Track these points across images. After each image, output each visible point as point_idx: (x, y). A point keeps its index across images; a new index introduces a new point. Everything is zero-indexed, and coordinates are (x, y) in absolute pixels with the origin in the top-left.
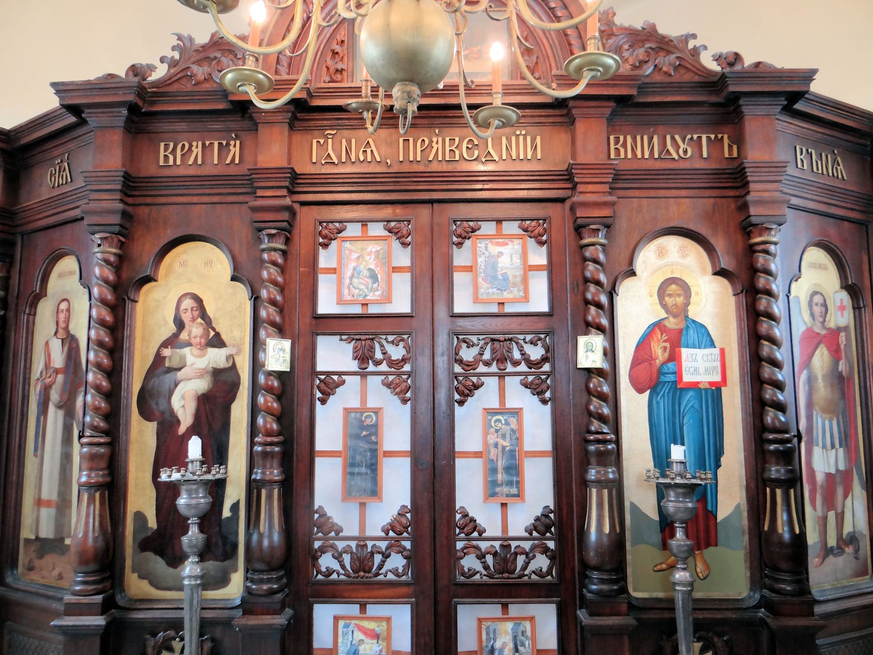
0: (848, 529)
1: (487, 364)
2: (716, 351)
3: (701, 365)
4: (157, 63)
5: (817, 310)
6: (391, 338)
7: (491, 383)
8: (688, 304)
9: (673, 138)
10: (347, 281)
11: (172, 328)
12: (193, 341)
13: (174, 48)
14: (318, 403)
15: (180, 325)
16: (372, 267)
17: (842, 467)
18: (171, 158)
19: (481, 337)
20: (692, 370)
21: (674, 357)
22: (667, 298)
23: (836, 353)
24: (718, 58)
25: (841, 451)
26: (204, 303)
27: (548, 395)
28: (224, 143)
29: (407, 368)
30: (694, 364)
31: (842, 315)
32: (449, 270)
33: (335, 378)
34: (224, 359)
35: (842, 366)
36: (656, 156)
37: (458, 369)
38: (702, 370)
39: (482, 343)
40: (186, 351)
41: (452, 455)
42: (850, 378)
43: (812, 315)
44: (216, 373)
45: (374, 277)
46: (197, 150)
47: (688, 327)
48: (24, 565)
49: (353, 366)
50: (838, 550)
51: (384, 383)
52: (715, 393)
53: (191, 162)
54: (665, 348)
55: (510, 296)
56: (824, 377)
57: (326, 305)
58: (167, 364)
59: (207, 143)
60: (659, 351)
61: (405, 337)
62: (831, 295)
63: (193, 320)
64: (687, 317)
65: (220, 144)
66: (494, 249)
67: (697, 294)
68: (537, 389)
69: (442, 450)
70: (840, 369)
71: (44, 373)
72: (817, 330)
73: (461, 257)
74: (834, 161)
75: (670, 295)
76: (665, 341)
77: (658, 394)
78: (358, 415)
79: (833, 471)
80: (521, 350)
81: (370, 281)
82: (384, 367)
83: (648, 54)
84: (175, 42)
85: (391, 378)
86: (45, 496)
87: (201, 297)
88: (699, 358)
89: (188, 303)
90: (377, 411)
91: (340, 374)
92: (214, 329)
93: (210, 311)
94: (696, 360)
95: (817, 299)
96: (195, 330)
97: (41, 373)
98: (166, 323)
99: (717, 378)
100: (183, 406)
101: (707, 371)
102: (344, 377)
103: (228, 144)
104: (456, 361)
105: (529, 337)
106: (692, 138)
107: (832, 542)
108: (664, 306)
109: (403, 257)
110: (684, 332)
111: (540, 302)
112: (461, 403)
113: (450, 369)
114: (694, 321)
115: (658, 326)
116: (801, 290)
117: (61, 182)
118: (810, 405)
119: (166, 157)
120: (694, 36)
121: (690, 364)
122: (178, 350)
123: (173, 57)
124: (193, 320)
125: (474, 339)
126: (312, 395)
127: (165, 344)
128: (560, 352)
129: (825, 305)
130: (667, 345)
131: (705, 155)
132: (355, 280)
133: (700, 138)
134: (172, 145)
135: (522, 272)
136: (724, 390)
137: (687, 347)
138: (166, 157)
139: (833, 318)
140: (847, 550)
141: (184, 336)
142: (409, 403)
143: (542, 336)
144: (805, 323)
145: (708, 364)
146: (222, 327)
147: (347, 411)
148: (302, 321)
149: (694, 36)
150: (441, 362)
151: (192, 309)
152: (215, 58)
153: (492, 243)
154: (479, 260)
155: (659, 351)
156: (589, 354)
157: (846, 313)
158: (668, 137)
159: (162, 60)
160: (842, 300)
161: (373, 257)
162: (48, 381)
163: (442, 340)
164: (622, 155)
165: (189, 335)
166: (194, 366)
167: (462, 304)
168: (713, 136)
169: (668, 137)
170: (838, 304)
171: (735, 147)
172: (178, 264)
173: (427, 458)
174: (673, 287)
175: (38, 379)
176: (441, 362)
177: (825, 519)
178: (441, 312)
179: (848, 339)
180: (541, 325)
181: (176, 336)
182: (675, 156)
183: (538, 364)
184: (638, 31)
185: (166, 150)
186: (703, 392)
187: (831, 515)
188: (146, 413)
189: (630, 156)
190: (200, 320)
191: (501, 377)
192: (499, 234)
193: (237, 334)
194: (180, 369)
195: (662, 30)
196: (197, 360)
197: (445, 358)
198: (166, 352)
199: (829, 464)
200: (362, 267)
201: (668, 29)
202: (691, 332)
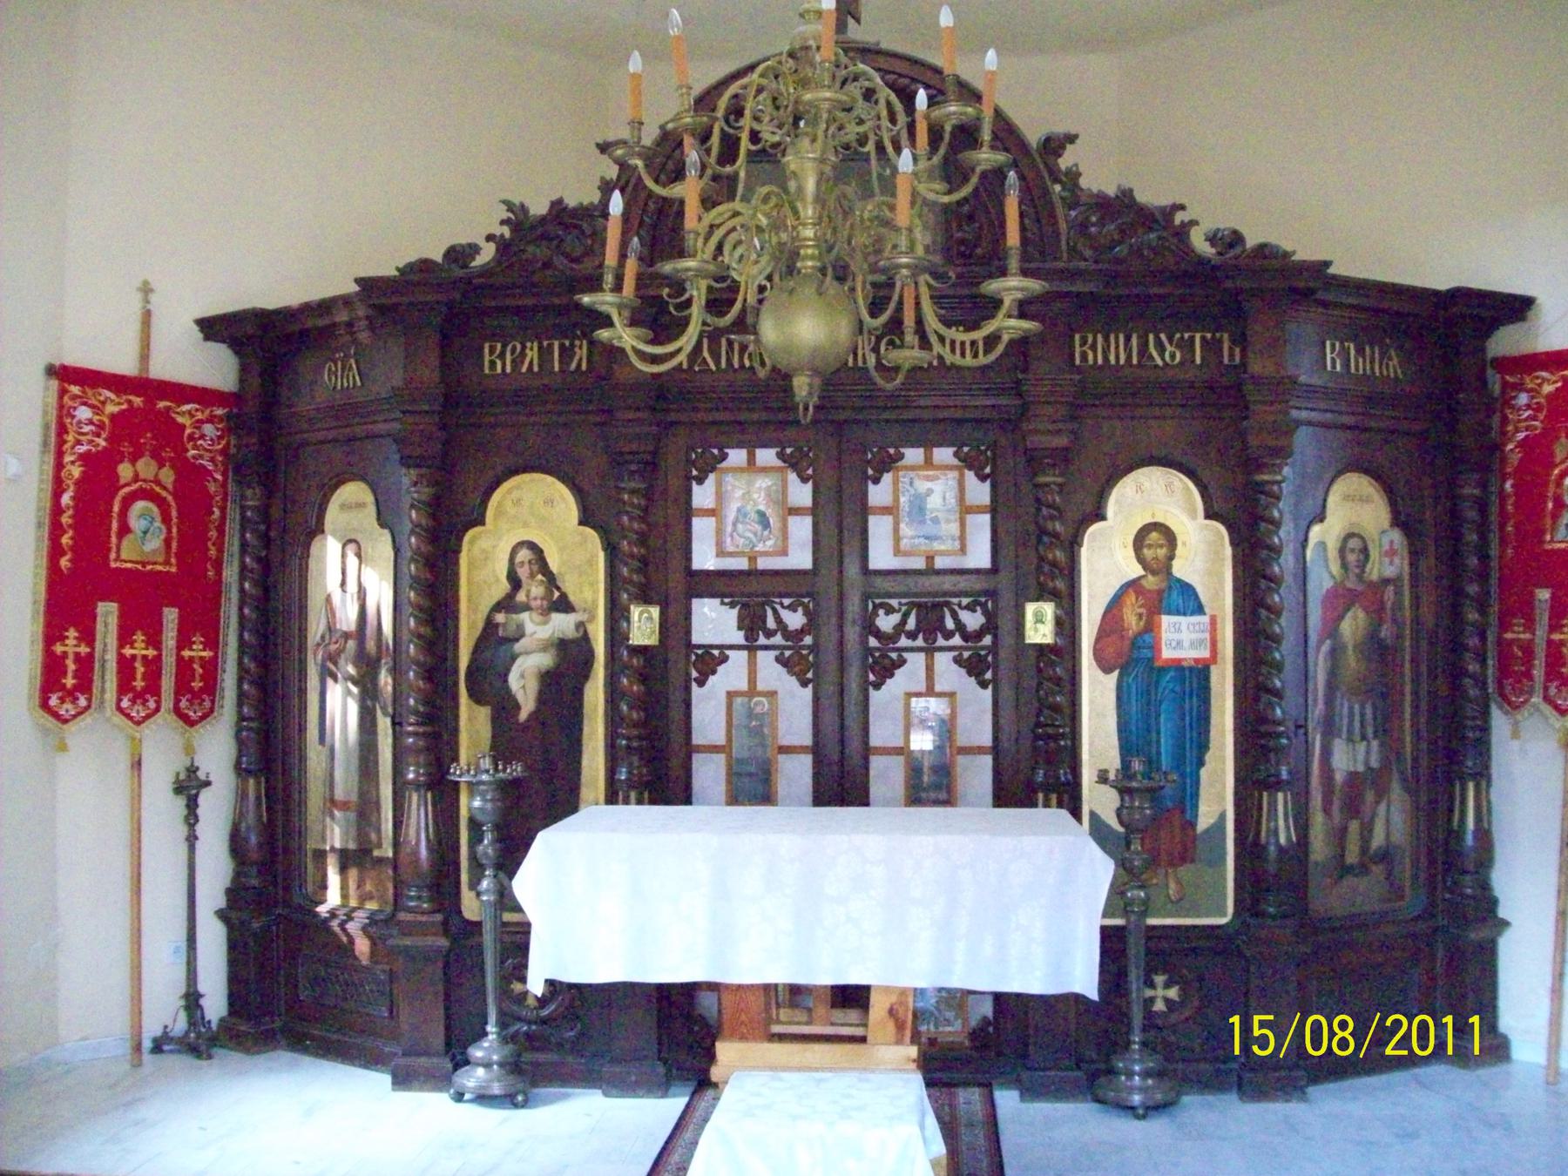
0: (1378, 840)
1: (912, 635)
2: (1205, 619)
3: (1186, 636)
4: (482, 243)
5: (1352, 558)
6: (787, 602)
7: (916, 661)
8: (1171, 557)
9: (1158, 339)
10: (729, 529)
11: (504, 587)
12: (534, 604)
13: (503, 222)
14: (694, 685)
15: (515, 582)
16: (762, 508)
17: (1375, 764)
18: (499, 364)
19: (904, 601)
20: (1174, 644)
21: (1151, 627)
22: (1145, 551)
23: (1377, 612)
24: (1212, 239)
25: (1375, 744)
26: (546, 554)
27: (988, 675)
28: (567, 343)
29: (808, 640)
30: (1176, 636)
31: (1391, 563)
32: (864, 510)
33: (716, 652)
34: (572, 627)
35: (1386, 632)
36: (1135, 361)
37: (873, 642)
38: (1186, 644)
39: (904, 608)
40: (525, 616)
41: (867, 751)
42: (1396, 650)
43: (1344, 565)
44: (562, 645)
45: (763, 519)
46: (532, 354)
47: (1170, 588)
48: (314, 883)
49: (738, 637)
50: (1363, 869)
51: (778, 659)
52: (1197, 677)
53: (524, 370)
54: (1140, 616)
55: (943, 547)
56: (1355, 647)
57: (705, 558)
58: (501, 633)
59: (545, 343)
60: (1132, 619)
61: (806, 600)
62: (1376, 537)
63: (532, 576)
64: (1169, 573)
65: (562, 346)
66: (922, 486)
67: (1184, 544)
68: (974, 667)
69: (854, 745)
70: (1383, 635)
71: (327, 637)
72: (1349, 585)
73: (878, 494)
74: (1383, 355)
75: (1150, 546)
76: (1140, 607)
77: (1130, 675)
78: (746, 699)
79: (1361, 768)
80: (955, 616)
81: (758, 528)
82: (778, 639)
83: (1122, 231)
84: (506, 215)
85: (787, 653)
86: (339, 794)
87: (541, 546)
88: (1184, 627)
89: (524, 555)
90: (772, 694)
91: (721, 647)
92: (558, 588)
93: (554, 564)
94: (1179, 630)
95: (1354, 543)
96: (534, 589)
97: (323, 637)
98: (498, 580)
99: (1205, 653)
100: (524, 687)
101: (1193, 645)
102: (727, 652)
103: (572, 345)
104: (871, 633)
105: (965, 601)
106: (1182, 338)
107: (1352, 857)
108: (1140, 559)
109: (802, 494)
110: (1166, 595)
111: (979, 555)
112: (877, 686)
113: (864, 642)
114: (1179, 581)
115: (1133, 585)
116: (1328, 534)
117: (346, 384)
118: (1331, 687)
119: (493, 364)
120: (1182, 207)
121: (1171, 636)
122: (514, 616)
123: (502, 236)
124: (532, 576)
125: (894, 602)
126: (688, 674)
127: (499, 607)
128: (1005, 624)
129: (1365, 551)
130: (1142, 610)
131: (1198, 361)
132: (740, 527)
133: (1192, 339)
134: (499, 346)
135: (958, 516)
136: (1213, 669)
137: (1169, 613)
138: (493, 364)
139: (1377, 565)
140: (1374, 868)
141: (521, 597)
142: (810, 686)
143: (983, 600)
144: (1333, 577)
145: (1194, 636)
146: (571, 586)
147: (731, 695)
148: (676, 581)
149: (1182, 207)
150: (852, 633)
151: (530, 562)
152: (558, 236)
153: (919, 476)
154: (902, 499)
155: (1132, 619)
156: (1039, 625)
157: (1397, 561)
158: (1151, 337)
159: (490, 238)
160: (1392, 542)
161: (763, 494)
162: (333, 647)
163: (853, 607)
164: (1091, 361)
165: (527, 596)
166: (536, 636)
167: (881, 557)
168: (1209, 336)
169: (1151, 337)
170: (1386, 547)
171: (1237, 350)
172: (510, 503)
173: (833, 751)
174: (1154, 535)
175: (318, 645)
176: (852, 633)
177: (1344, 830)
178: (852, 570)
179: (1398, 593)
180: (977, 584)
181: (510, 596)
182: (1159, 362)
183: (979, 635)
184: (1110, 198)
185: (492, 352)
186: (1187, 673)
187: (1354, 826)
188: (477, 697)
189: (1100, 361)
190: (540, 577)
191: (930, 651)
192: (928, 462)
193: (588, 594)
194: (517, 640)
195: (1142, 197)
196: (539, 629)
197: (857, 629)
198: (500, 618)
199: (1355, 761)
200: (749, 508)
201: (1150, 195)
202: (1175, 594)
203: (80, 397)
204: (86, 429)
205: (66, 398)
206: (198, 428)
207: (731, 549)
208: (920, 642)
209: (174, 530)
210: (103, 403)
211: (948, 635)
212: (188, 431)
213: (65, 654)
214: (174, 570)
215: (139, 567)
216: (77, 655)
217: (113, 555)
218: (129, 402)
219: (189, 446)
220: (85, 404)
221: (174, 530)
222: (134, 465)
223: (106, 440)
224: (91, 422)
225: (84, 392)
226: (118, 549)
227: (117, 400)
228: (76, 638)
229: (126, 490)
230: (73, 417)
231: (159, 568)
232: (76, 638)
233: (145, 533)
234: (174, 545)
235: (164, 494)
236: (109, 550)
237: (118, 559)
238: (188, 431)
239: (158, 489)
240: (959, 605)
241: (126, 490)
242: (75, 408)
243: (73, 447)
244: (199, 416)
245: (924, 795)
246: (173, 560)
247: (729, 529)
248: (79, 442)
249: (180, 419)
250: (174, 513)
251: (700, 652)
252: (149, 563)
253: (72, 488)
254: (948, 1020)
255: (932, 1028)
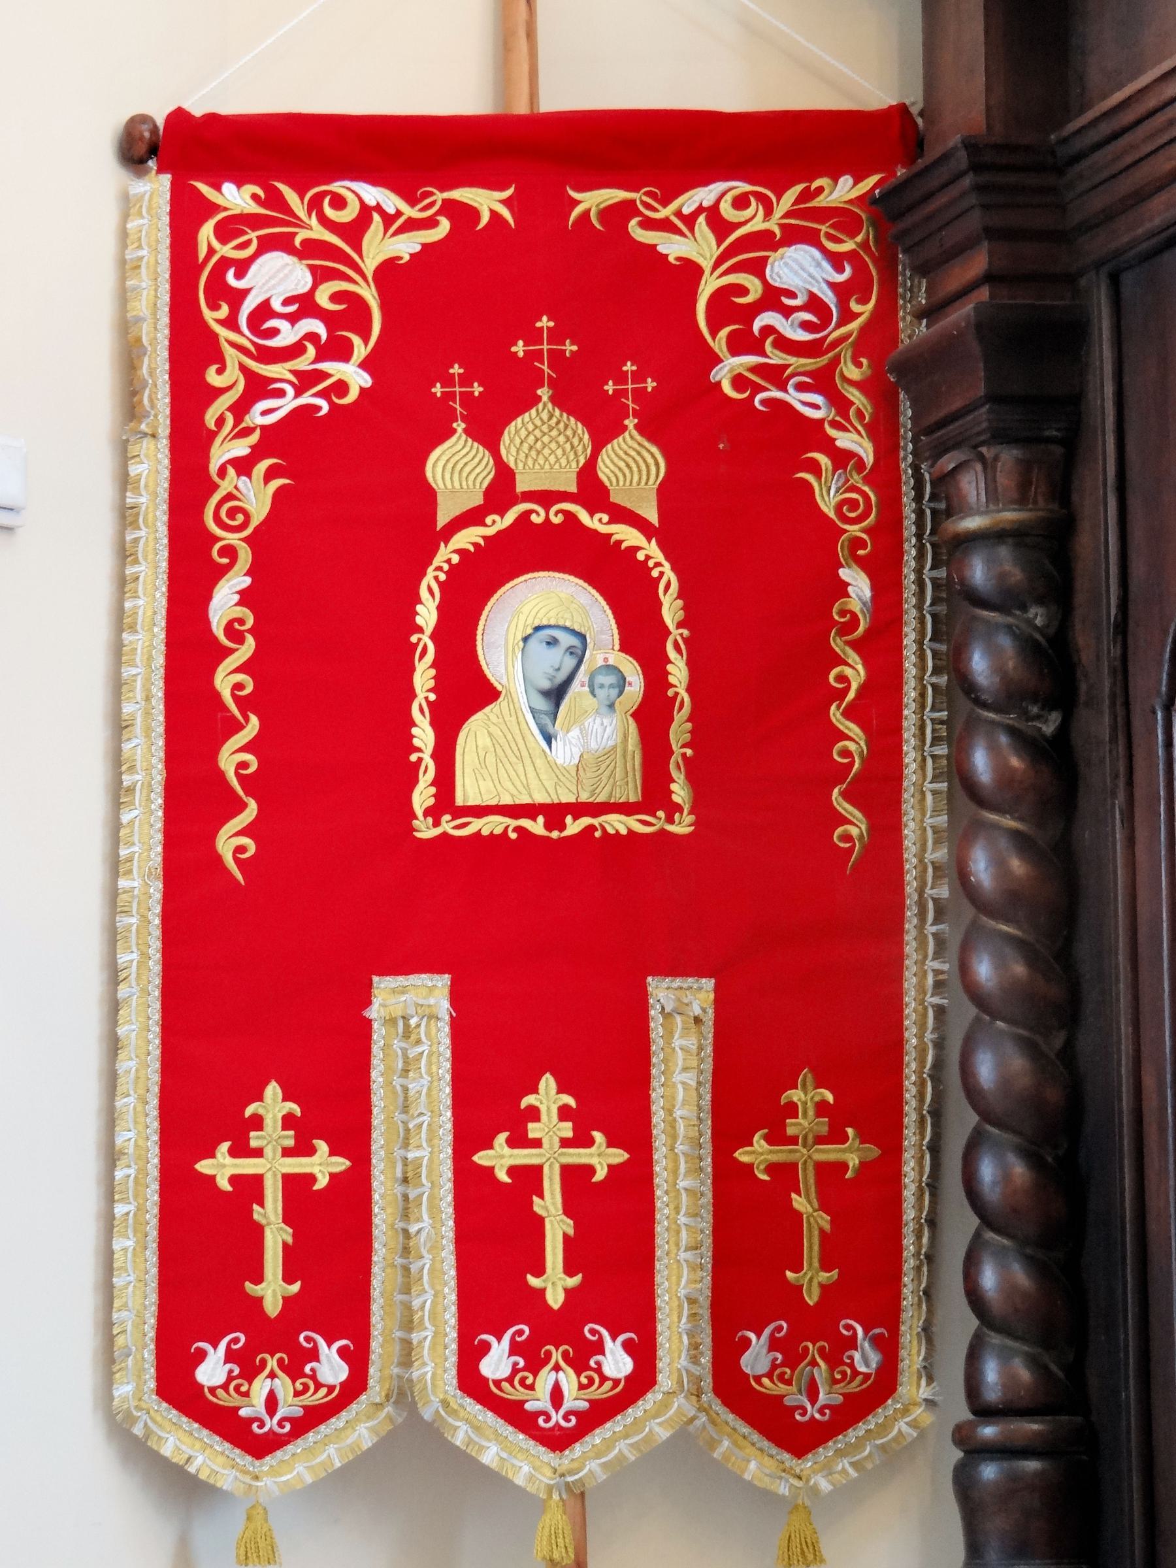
203: (253, 221)
204: (288, 335)
205: (207, 232)
206: (757, 268)
209: (678, 672)
210: (354, 232)
212: (709, 286)
213: (250, 1188)
214: (682, 826)
215: (537, 827)
216: (296, 1185)
217: (422, 796)
218: (462, 214)
219: (719, 343)
220: (283, 244)
221: (678, 672)
222: (491, 441)
223: (364, 365)
224: (305, 305)
225: (274, 200)
226: (445, 781)
227: (410, 212)
228: (564, 1113)
229: (467, 538)
230: (237, 298)
231: (617, 824)
232: (288, 1121)
233: (557, 694)
234: (679, 732)
235: (628, 535)
236: (411, 774)
237: (444, 802)
238: (709, 286)
239: (596, 522)
241: (467, 538)
242: (242, 268)
243: (240, 409)
244: (755, 221)
246: (680, 792)
248: (258, 388)
249: (673, 247)
250: (671, 610)
252: (579, 809)
253: (245, 556)
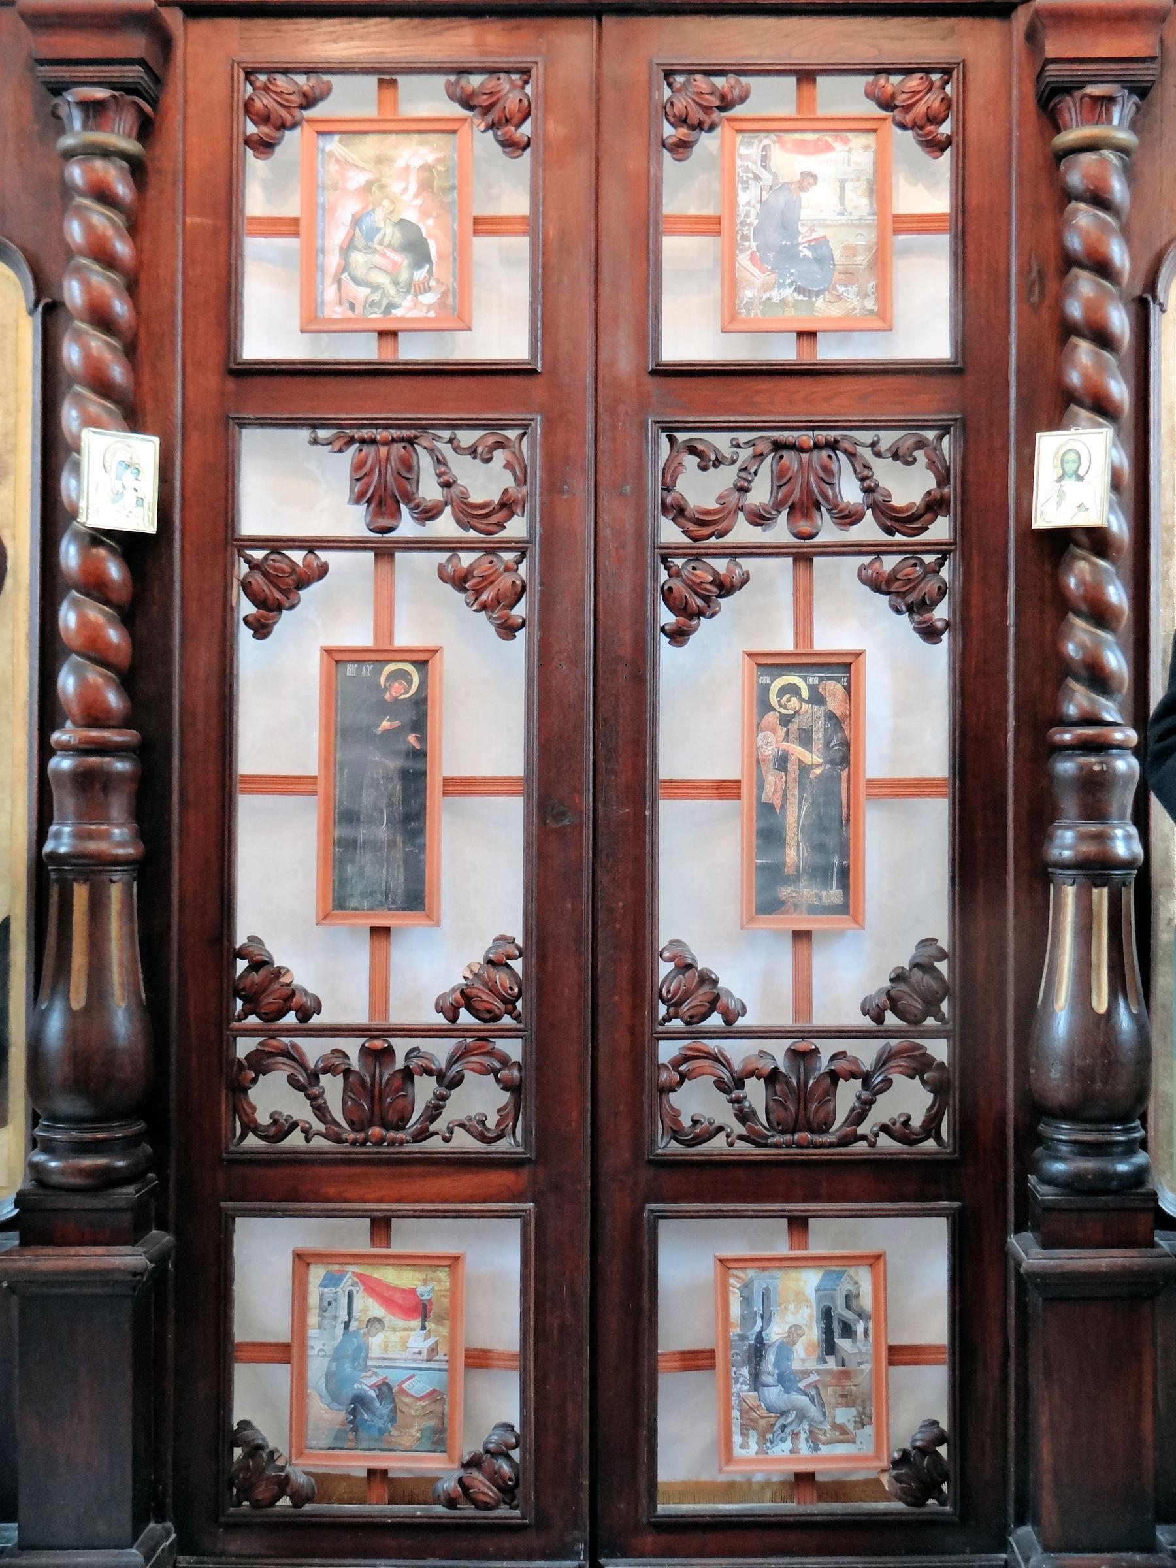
1: (759, 518)
6: (467, 437)
14: (245, 634)
16: (411, 216)
19: (743, 437)
45: (417, 250)
55: (836, 311)
90: (423, 661)
91: (311, 545)
132: (357, 258)
147: (336, 658)
154: (743, 197)
156: (1069, 484)
200: (379, 217)
207: (334, 311)
208: (827, 1048)
211: (849, 518)
240: (308, 1133)
245: (785, 892)
247: (332, 261)
251: (258, 555)
254: (842, 1429)
255: (804, 1448)
